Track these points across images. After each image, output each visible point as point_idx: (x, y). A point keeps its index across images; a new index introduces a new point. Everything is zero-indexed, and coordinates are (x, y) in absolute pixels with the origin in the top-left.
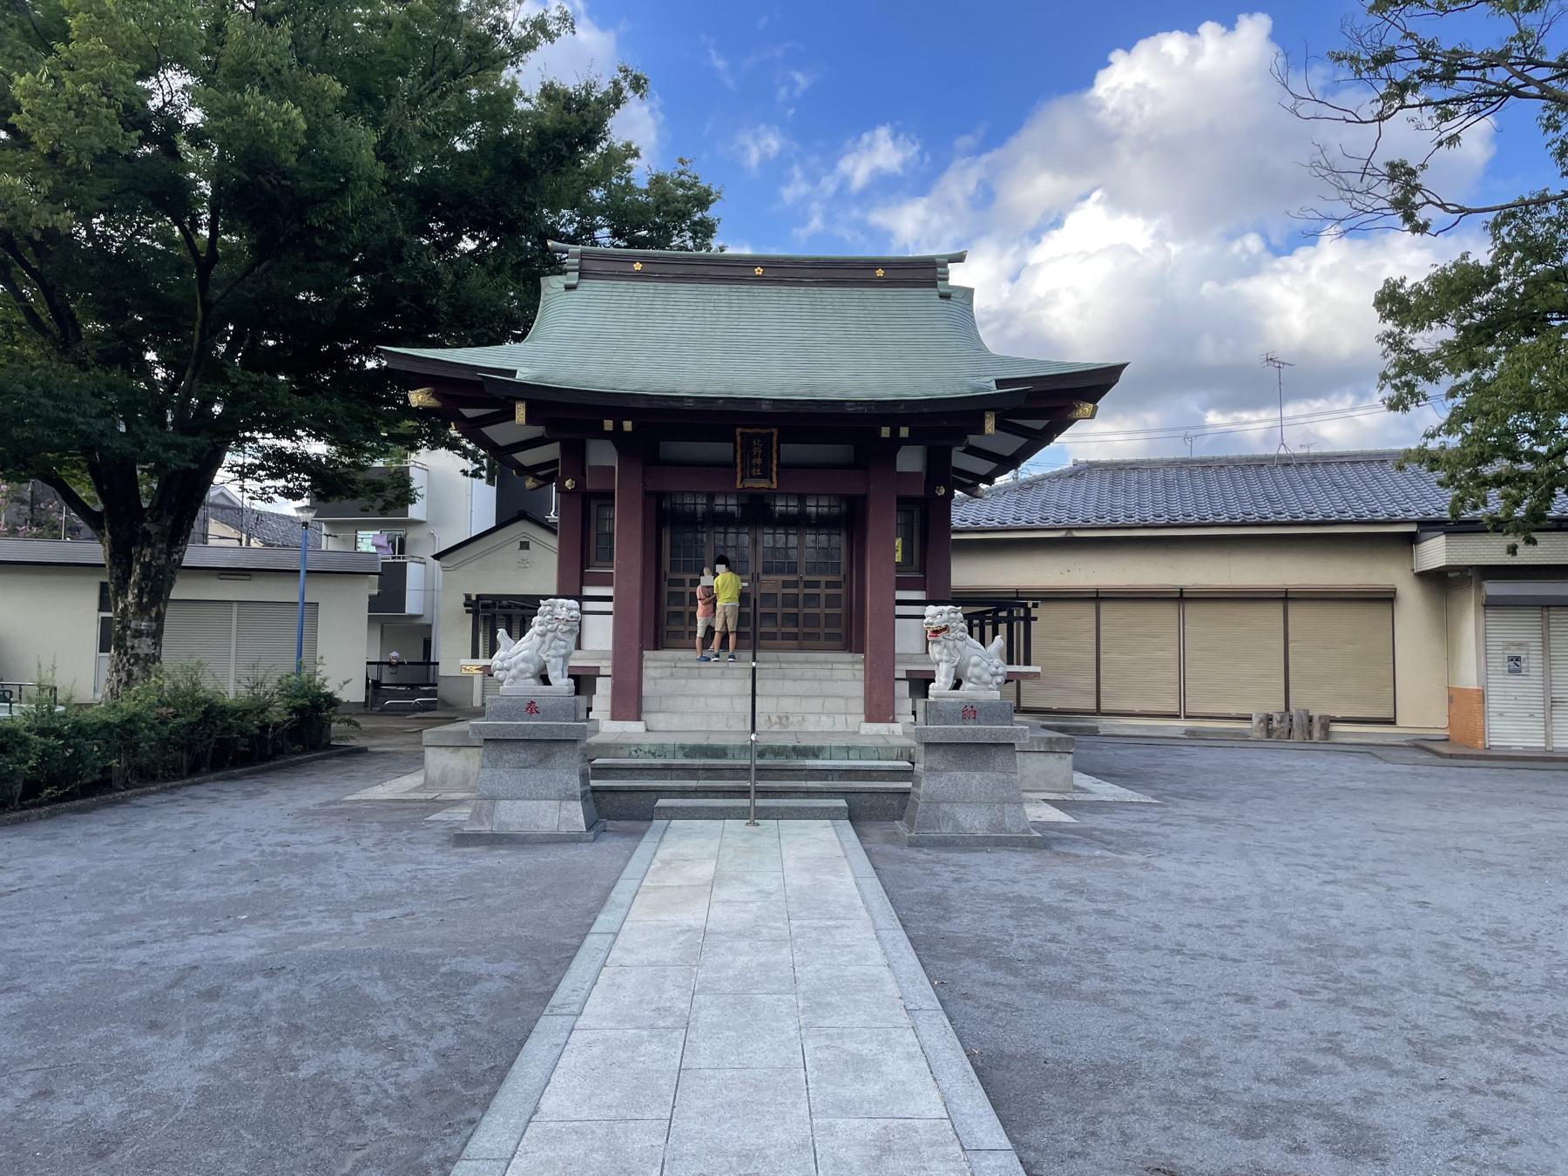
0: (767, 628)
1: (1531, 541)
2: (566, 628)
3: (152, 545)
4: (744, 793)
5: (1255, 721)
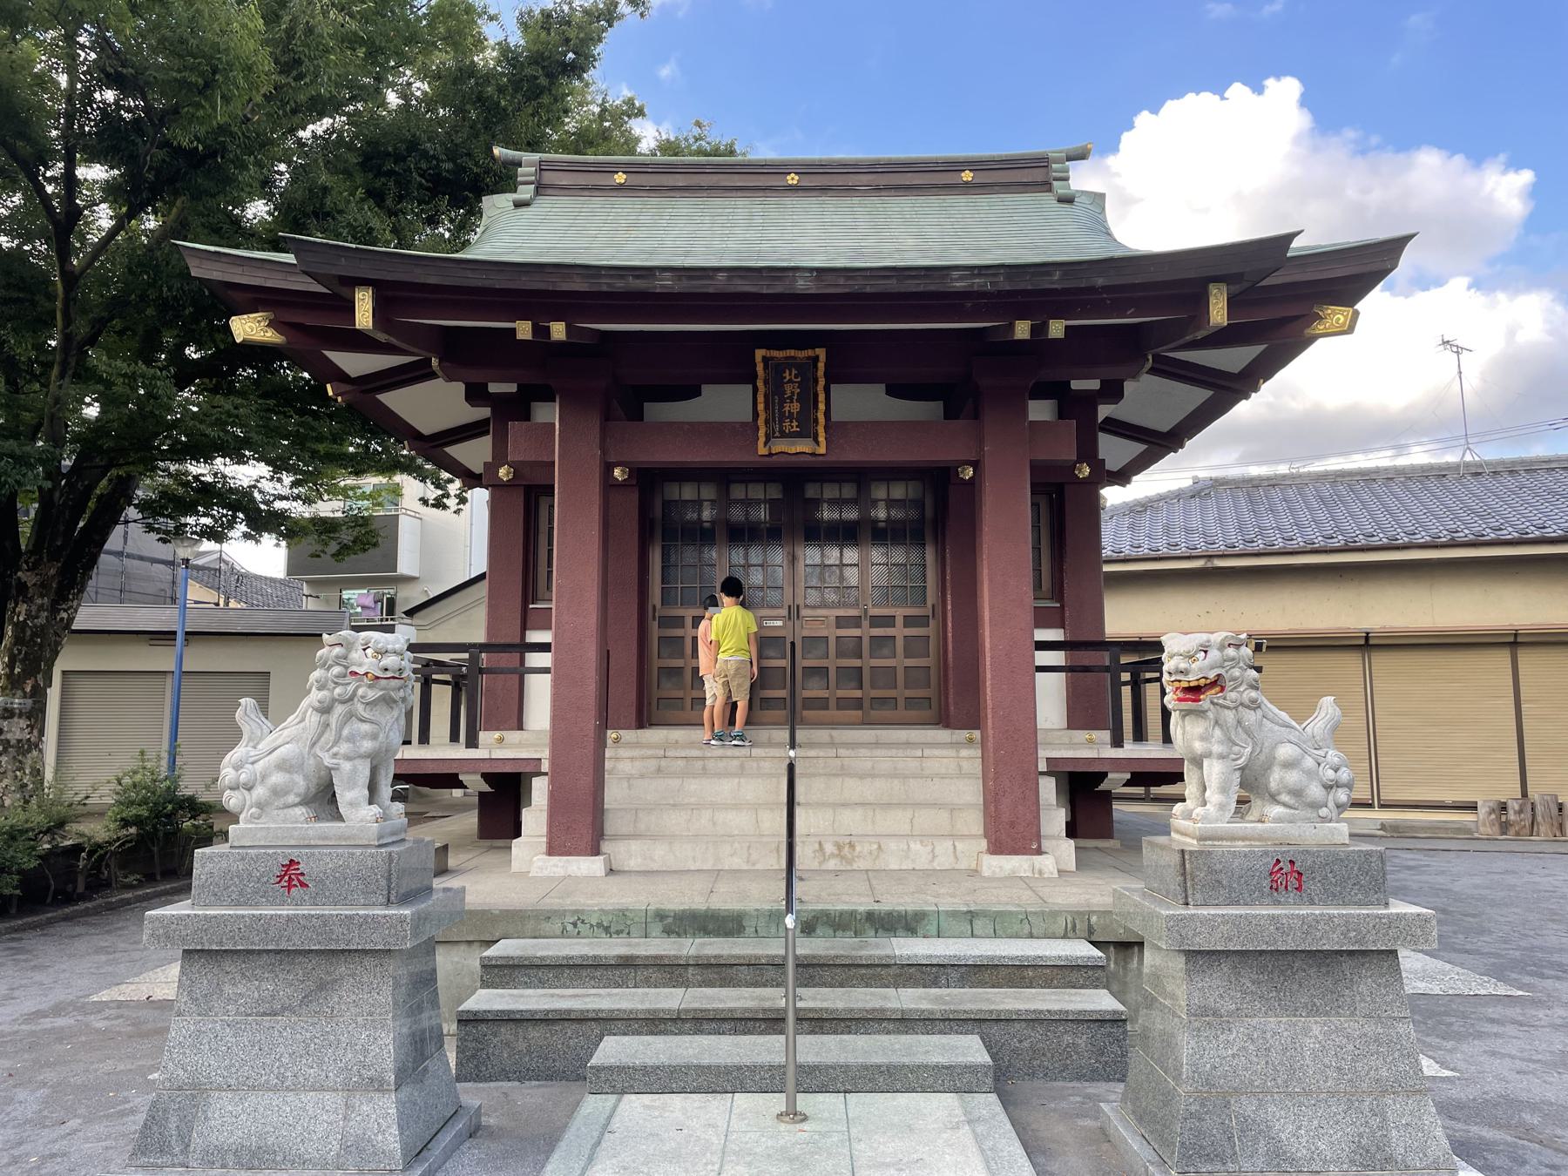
0: (814, 691)
2: (372, 694)
3: (29, 600)
4: (771, 1022)
5: (1482, 811)
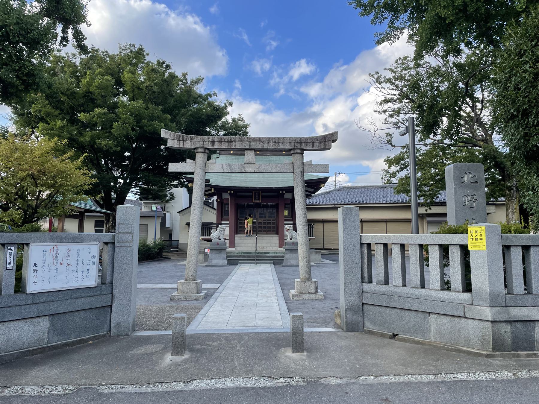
1: (430, 209)
